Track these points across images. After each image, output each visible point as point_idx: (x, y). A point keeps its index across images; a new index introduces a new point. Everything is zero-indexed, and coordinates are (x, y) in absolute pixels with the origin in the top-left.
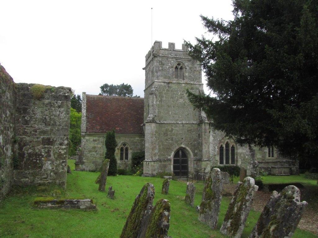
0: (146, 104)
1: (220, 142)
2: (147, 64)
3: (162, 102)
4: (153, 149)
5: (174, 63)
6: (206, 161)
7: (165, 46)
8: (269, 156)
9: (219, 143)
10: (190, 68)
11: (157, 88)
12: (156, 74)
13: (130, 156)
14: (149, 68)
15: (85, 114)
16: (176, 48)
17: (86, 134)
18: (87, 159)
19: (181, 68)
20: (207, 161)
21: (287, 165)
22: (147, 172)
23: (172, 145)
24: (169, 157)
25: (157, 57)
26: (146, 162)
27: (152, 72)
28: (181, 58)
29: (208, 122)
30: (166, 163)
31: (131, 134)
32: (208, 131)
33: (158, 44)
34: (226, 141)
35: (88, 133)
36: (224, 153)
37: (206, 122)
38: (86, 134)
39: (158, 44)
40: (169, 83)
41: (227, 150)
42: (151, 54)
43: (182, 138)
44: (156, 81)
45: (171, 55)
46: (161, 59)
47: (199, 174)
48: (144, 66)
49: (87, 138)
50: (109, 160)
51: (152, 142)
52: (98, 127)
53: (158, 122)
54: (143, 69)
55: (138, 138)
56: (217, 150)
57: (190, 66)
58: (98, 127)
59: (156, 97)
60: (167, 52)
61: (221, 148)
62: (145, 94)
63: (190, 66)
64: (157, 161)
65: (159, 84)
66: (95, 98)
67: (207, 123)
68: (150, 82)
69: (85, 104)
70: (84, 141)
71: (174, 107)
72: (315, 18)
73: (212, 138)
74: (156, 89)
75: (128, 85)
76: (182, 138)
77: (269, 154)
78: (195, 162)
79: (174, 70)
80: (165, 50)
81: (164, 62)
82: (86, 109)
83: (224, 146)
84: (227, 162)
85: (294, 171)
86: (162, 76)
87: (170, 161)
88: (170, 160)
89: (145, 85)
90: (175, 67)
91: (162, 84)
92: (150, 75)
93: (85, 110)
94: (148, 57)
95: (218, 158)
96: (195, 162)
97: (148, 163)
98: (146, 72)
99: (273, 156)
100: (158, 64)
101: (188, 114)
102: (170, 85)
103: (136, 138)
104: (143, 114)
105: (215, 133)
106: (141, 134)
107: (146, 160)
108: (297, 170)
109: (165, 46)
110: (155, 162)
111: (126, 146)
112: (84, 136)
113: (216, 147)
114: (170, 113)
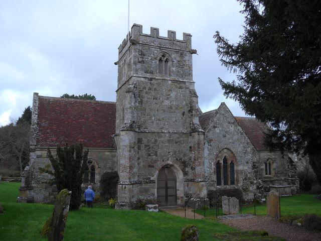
0: (119, 108)
1: (217, 156)
2: (121, 56)
3: (142, 104)
4: (131, 167)
5: (157, 53)
6: (201, 182)
7: (146, 31)
8: (266, 174)
9: (216, 158)
10: (178, 61)
11: (135, 84)
12: (134, 66)
13: (97, 177)
14: (123, 61)
15: (36, 121)
16: (160, 35)
17: (36, 147)
18: (38, 182)
19: (167, 61)
20: (203, 181)
21: (286, 183)
22: (123, 200)
23: (156, 161)
24: (152, 178)
25: (135, 44)
26: (121, 186)
27: (129, 65)
28: (166, 48)
29: (203, 131)
30: (148, 186)
31: (99, 147)
32: (203, 142)
33: (137, 28)
34: (224, 156)
35: (39, 146)
36: (222, 171)
37: (200, 130)
38: (36, 147)
39: (137, 28)
40: (151, 79)
41: (225, 167)
42: (127, 41)
43: (169, 152)
44: (135, 75)
45: (154, 43)
46: (141, 48)
47: (192, 199)
48: (117, 60)
49: (38, 153)
50: (70, 192)
51: (130, 158)
52: (54, 139)
53: (137, 130)
54: (116, 64)
55: (108, 153)
56: (213, 167)
57: (178, 59)
58: (54, 139)
59: (135, 97)
60: (148, 39)
61: (218, 165)
62: (117, 96)
63: (178, 59)
64: (136, 183)
65: (139, 79)
66: (51, 101)
67: (202, 132)
68: (124, 79)
69: (37, 108)
70: (33, 156)
71: (158, 111)
72: (53, 206)
73: (208, 152)
74: (134, 87)
75: (92, 96)
76: (169, 152)
77: (266, 171)
78: (186, 184)
79: (158, 63)
80: (146, 36)
81: (145, 52)
82: (38, 115)
83: (222, 162)
84: (226, 183)
85: (294, 191)
86: (142, 69)
87: (153, 183)
88: (153, 182)
89: (117, 84)
90: (158, 58)
91: (143, 79)
92: (125, 73)
93: (37, 116)
94: (122, 48)
95: (214, 177)
96: (186, 184)
97: (124, 186)
98: (119, 67)
99: (270, 174)
100: (137, 54)
101: (176, 121)
102: (152, 82)
103: (106, 153)
104: (115, 121)
105: (211, 146)
106: (112, 146)
107: (121, 182)
108: (297, 190)
109: (146, 31)
110: (134, 185)
111: (93, 164)
112: (34, 151)
113: (213, 163)
114: (153, 118)
